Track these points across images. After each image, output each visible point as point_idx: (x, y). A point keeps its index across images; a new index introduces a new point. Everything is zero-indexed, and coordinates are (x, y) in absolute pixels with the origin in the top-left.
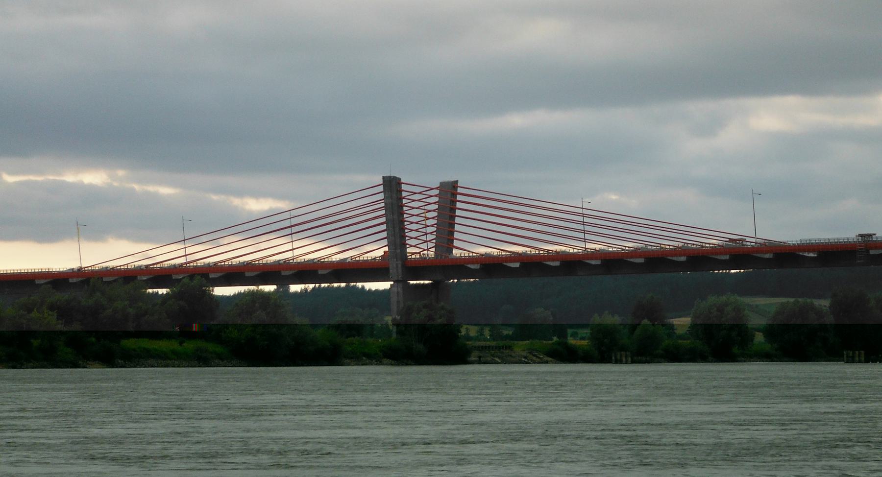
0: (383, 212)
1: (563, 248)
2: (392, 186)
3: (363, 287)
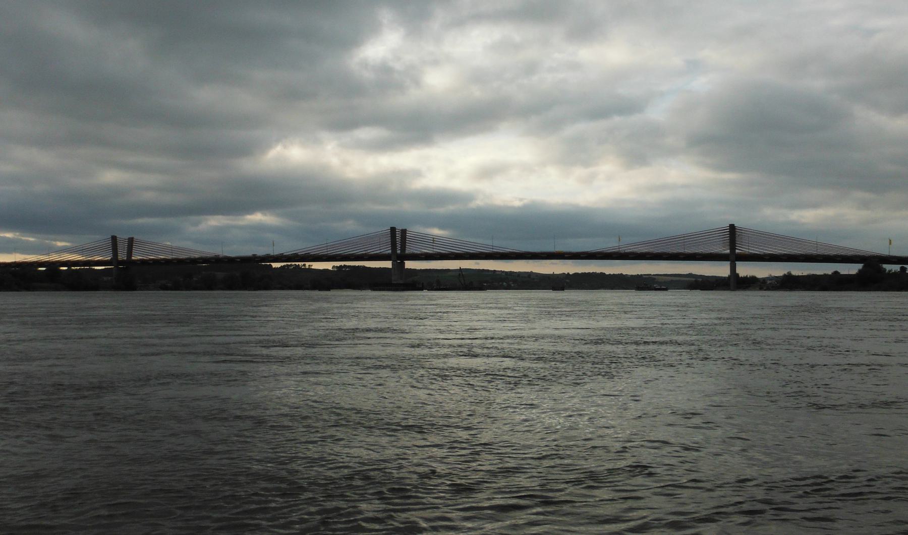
1: (428, 251)
2: (114, 238)
3: (270, 265)
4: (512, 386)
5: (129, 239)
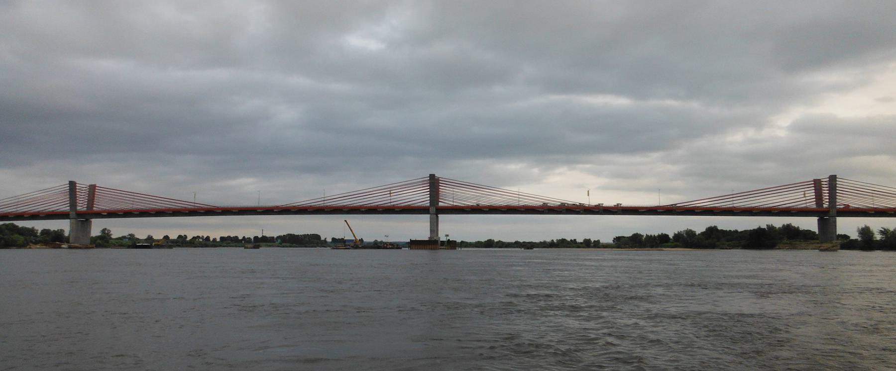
2: (72, 185)
4: (484, 305)
5: (91, 186)
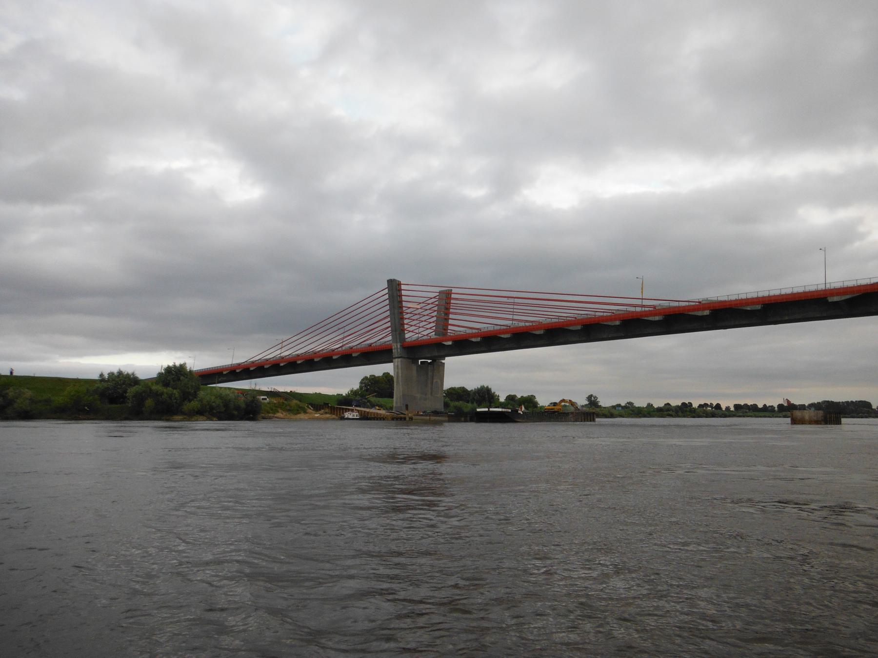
0: (389, 324)
